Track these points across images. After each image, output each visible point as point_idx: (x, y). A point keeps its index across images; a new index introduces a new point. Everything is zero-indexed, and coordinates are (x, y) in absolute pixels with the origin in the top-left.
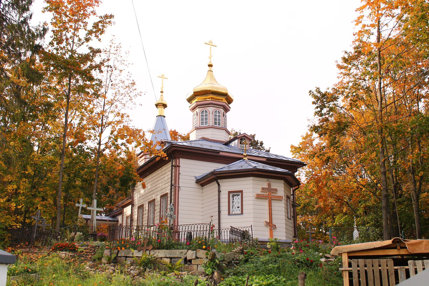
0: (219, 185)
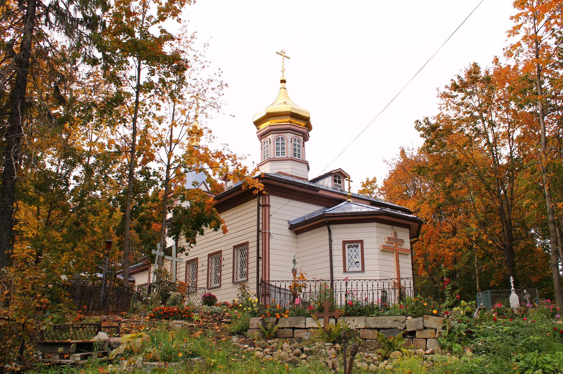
0: (330, 232)
